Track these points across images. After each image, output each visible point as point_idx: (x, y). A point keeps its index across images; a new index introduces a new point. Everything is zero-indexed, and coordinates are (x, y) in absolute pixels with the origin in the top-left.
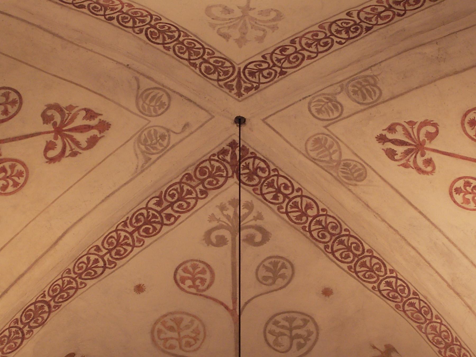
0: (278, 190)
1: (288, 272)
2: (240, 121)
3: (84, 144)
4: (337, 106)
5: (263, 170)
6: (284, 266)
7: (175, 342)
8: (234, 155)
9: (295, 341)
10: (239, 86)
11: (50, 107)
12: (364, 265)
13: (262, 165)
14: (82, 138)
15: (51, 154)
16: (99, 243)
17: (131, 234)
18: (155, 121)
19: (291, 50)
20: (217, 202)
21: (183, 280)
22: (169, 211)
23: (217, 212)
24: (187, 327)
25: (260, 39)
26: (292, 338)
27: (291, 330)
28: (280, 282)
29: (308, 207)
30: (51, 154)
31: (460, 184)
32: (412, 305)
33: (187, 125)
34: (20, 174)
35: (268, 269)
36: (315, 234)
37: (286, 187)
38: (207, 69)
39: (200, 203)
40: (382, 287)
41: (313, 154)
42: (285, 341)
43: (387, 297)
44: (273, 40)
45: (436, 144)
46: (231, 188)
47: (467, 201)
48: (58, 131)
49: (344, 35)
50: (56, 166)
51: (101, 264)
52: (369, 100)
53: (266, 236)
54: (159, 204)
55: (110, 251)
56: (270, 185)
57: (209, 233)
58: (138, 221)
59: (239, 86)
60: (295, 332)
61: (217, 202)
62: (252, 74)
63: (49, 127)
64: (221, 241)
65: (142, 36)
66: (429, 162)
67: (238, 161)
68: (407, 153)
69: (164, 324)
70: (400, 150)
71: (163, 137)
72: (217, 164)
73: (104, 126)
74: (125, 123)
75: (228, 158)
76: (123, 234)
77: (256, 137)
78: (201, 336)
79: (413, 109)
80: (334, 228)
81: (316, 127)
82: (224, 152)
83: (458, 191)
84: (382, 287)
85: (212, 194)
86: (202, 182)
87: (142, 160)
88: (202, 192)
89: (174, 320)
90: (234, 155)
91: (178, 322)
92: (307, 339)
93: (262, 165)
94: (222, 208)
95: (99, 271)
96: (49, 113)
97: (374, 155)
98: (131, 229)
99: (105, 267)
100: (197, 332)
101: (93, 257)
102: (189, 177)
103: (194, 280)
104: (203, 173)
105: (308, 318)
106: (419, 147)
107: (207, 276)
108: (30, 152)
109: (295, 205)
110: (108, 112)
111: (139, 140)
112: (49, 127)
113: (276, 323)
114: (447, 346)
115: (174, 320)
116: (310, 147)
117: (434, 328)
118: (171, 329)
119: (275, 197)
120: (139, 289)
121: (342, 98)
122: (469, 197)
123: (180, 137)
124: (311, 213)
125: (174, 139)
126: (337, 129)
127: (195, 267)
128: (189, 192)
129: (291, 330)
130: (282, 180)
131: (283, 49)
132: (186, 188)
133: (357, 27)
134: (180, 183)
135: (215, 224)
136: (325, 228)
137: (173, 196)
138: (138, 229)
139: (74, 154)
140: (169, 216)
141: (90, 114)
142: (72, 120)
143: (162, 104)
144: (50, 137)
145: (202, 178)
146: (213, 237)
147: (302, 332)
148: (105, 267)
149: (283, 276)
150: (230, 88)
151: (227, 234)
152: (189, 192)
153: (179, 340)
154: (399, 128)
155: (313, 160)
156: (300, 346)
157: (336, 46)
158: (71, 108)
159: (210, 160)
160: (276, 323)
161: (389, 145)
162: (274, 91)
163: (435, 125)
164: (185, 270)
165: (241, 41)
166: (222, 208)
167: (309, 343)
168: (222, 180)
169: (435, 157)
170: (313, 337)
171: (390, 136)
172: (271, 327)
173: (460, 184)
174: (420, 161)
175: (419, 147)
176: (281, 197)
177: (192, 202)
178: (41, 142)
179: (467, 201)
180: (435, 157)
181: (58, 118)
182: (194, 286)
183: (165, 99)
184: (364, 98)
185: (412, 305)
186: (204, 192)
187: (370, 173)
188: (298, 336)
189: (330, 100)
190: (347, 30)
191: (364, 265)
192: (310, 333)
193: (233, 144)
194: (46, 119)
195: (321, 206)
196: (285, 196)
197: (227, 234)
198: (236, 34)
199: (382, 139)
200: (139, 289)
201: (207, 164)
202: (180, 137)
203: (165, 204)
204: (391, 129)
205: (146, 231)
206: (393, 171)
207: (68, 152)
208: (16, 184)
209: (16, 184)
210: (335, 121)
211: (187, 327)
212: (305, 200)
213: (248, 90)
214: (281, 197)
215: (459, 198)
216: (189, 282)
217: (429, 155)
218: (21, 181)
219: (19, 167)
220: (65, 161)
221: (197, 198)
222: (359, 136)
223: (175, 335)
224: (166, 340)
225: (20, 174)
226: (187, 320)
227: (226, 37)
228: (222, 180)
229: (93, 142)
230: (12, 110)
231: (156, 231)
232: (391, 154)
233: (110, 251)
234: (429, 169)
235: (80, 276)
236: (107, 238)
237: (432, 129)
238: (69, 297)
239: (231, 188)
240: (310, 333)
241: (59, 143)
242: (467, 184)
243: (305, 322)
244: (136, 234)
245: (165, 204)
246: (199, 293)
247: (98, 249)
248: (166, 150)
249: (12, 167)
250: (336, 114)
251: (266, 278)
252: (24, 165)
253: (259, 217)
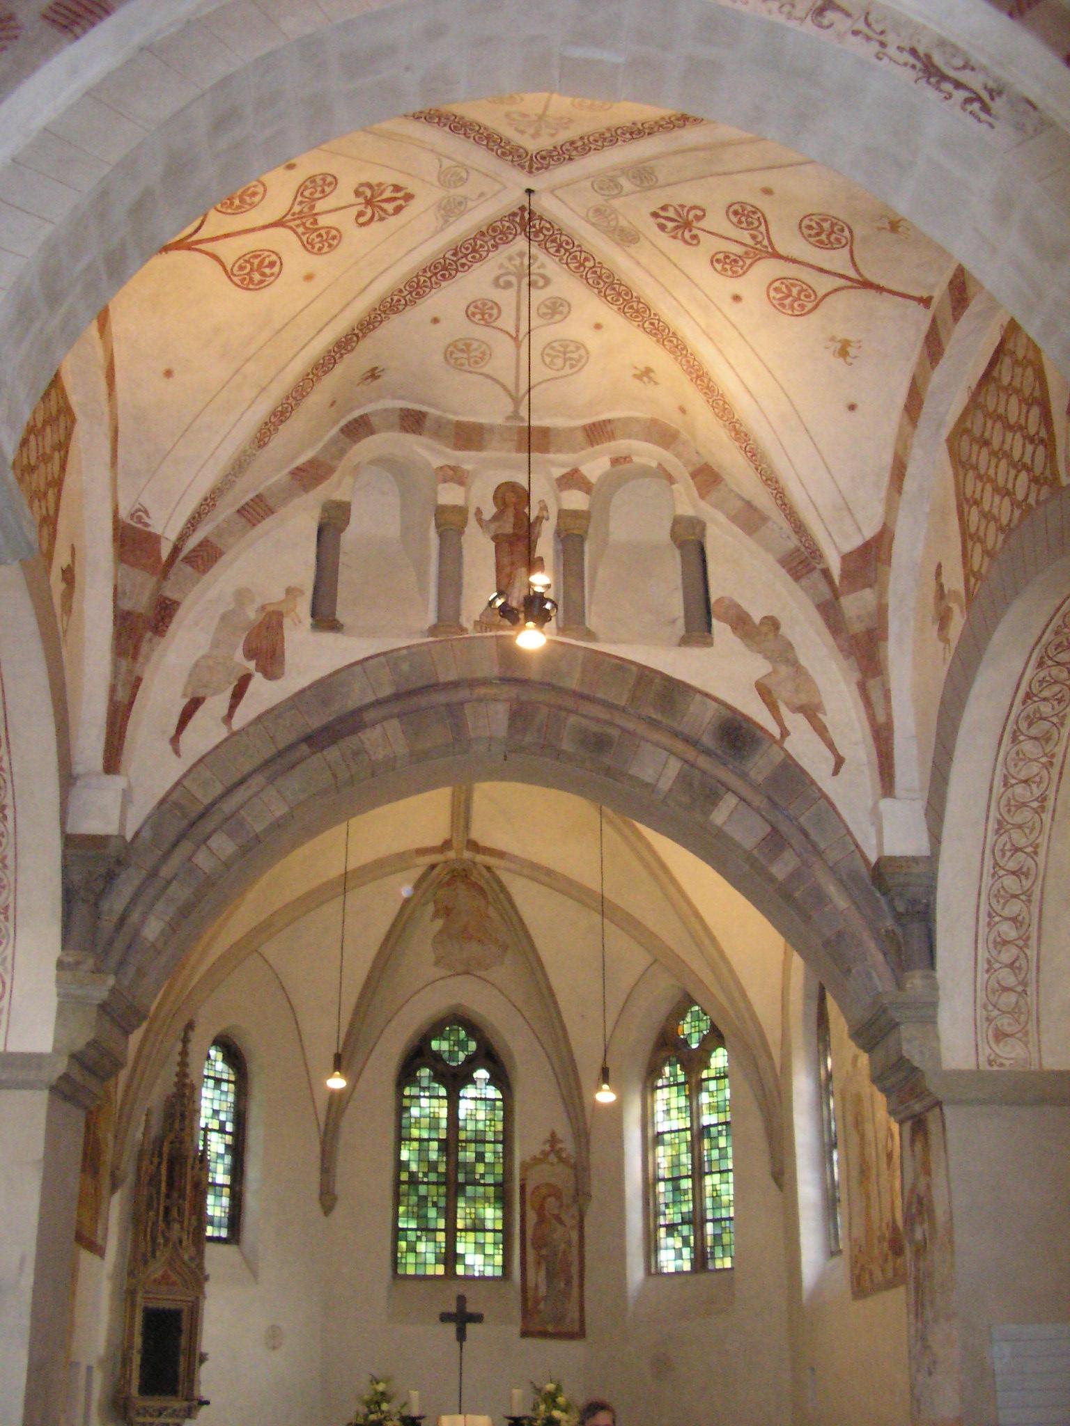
0: (560, 246)
1: (565, 310)
2: (529, 191)
3: (391, 210)
4: (619, 186)
5: (548, 230)
6: (561, 305)
7: (463, 361)
8: (522, 218)
9: (568, 363)
10: (531, 167)
11: (362, 185)
12: (631, 307)
13: (548, 225)
14: (390, 207)
15: (362, 220)
16: (402, 287)
17: (430, 278)
18: (453, 191)
19: (579, 143)
20: (506, 254)
21: (474, 314)
22: (464, 261)
23: (507, 264)
24: (475, 350)
25: (552, 135)
26: (565, 360)
27: (565, 353)
28: (558, 317)
29: (586, 259)
30: (362, 220)
31: (721, 256)
32: (671, 341)
33: (482, 194)
34: (334, 238)
35: (546, 306)
36: (591, 281)
37: (567, 243)
38: (504, 154)
39: (491, 254)
40: (646, 325)
41: (593, 220)
42: (559, 362)
43: (650, 333)
44: (565, 136)
45: (702, 224)
46: (521, 243)
47: (726, 270)
48: (369, 202)
49: (628, 136)
50: (364, 230)
51: (403, 302)
52: (646, 184)
53: (547, 281)
54: (454, 255)
55: (410, 293)
56: (554, 241)
57: (497, 278)
58: (436, 268)
59: (531, 167)
60: (568, 355)
61: (506, 254)
62: (543, 158)
63: (361, 200)
64: (508, 285)
65: (447, 128)
66: (694, 237)
67: (527, 221)
68: (677, 228)
69: (455, 347)
70: (670, 225)
71: (460, 203)
72: (507, 224)
73: (409, 197)
74: (427, 198)
75: (518, 219)
76: (422, 279)
77: (546, 204)
78: (487, 357)
79: (689, 195)
80: (608, 277)
81: (598, 200)
82: (514, 214)
83: (718, 261)
84: (646, 325)
85: (501, 248)
86: (494, 238)
87: (441, 221)
88: (493, 246)
89: (466, 344)
90: (522, 218)
91: (468, 346)
92: (579, 361)
93: (548, 225)
94: (510, 259)
95: (401, 307)
96: (361, 189)
97: (649, 227)
98: (429, 274)
99: (406, 305)
100: (484, 353)
101: (396, 298)
102: (482, 234)
103: (483, 315)
104: (494, 230)
105: (580, 346)
106: (687, 225)
107: (495, 312)
108: (344, 221)
109: (575, 257)
110: (411, 186)
111: (439, 207)
112: (361, 200)
113: (553, 348)
114: (698, 377)
115: (466, 344)
116: (591, 214)
117: (688, 362)
118: (462, 351)
119: (558, 251)
120: (436, 321)
121: (622, 180)
122: (728, 267)
123: (474, 204)
124: (588, 264)
125: (470, 204)
126: (615, 203)
127: (484, 304)
128: (481, 246)
129: (565, 353)
130: (564, 238)
131: (572, 143)
132: (479, 242)
133: (639, 131)
134: (474, 239)
135: (502, 271)
136: (600, 277)
137: (467, 249)
138: (436, 274)
139: (382, 219)
140: (463, 265)
141: (397, 188)
142: (381, 194)
143: (461, 179)
144: (361, 208)
145: (493, 235)
146: (501, 281)
147: (575, 356)
148: (406, 305)
149: (561, 313)
150: (523, 167)
151: (513, 279)
152: (481, 246)
153: (468, 359)
154: (671, 209)
155: (593, 224)
156: (572, 366)
157: (620, 143)
158: (380, 184)
159: (501, 220)
160: (553, 348)
161: (661, 221)
162: (562, 173)
163: (703, 210)
164: (476, 307)
165: (535, 136)
166: (510, 259)
167: (580, 365)
168: (511, 237)
169: (700, 233)
170: (583, 361)
171: (662, 214)
172: (548, 351)
173: (721, 256)
174: (687, 235)
175: (687, 225)
176: (563, 251)
177: (484, 254)
178: (354, 211)
179: (726, 270)
180: (701, 234)
181: (368, 193)
182: (483, 319)
183: (464, 175)
184: (642, 181)
185: (671, 341)
186: (495, 246)
187: (642, 239)
188: (571, 359)
189: (611, 181)
190: (631, 134)
191: (631, 307)
192: (581, 357)
193: (522, 209)
194: (357, 193)
195: (597, 260)
196: (566, 250)
197: (513, 279)
198: (532, 131)
199: (655, 215)
200: (436, 321)
201: (498, 224)
202: (474, 204)
203: (460, 255)
204: (664, 208)
205: (443, 276)
206: (663, 240)
207: (376, 217)
208: (330, 246)
209: (330, 246)
210: (614, 197)
211: (475, 350)
212: (583, 255)
213: (538, 169)
214: (563, 251)
215: (719, 267)
216: (479, 316)
217: (695, 232)
218: (335, 243)
219: (334, 232)
220: (374, 225)
221: (488, 251)
222: (635, 210)
223: (465, 356)
224: (456, 359)
225: (334, 238)
226: (475, 345)
227: (522, 132)
228: (511, 237)
229: (398, 210)
230: (327, 190)
231: (452, 277)
232: (662, 227)
233: (410, 293)
234: (695, 242)
235: (384, 312)
236: (409, 283)
237: (699, 213)
238: (375, 328)
239: (521, 243)
240: (581, 357)
241: (369, 212)
242: (727, 257)
243: (578, 348)
244: (434, 279)
245: (460, 255)
246: (487, 325)
247: (401, 291)
248: (462, 214)
249: (328, 233)
250: (616, 192)
251: (545, 314)
252: (337, 230)
253: (543, 266)
